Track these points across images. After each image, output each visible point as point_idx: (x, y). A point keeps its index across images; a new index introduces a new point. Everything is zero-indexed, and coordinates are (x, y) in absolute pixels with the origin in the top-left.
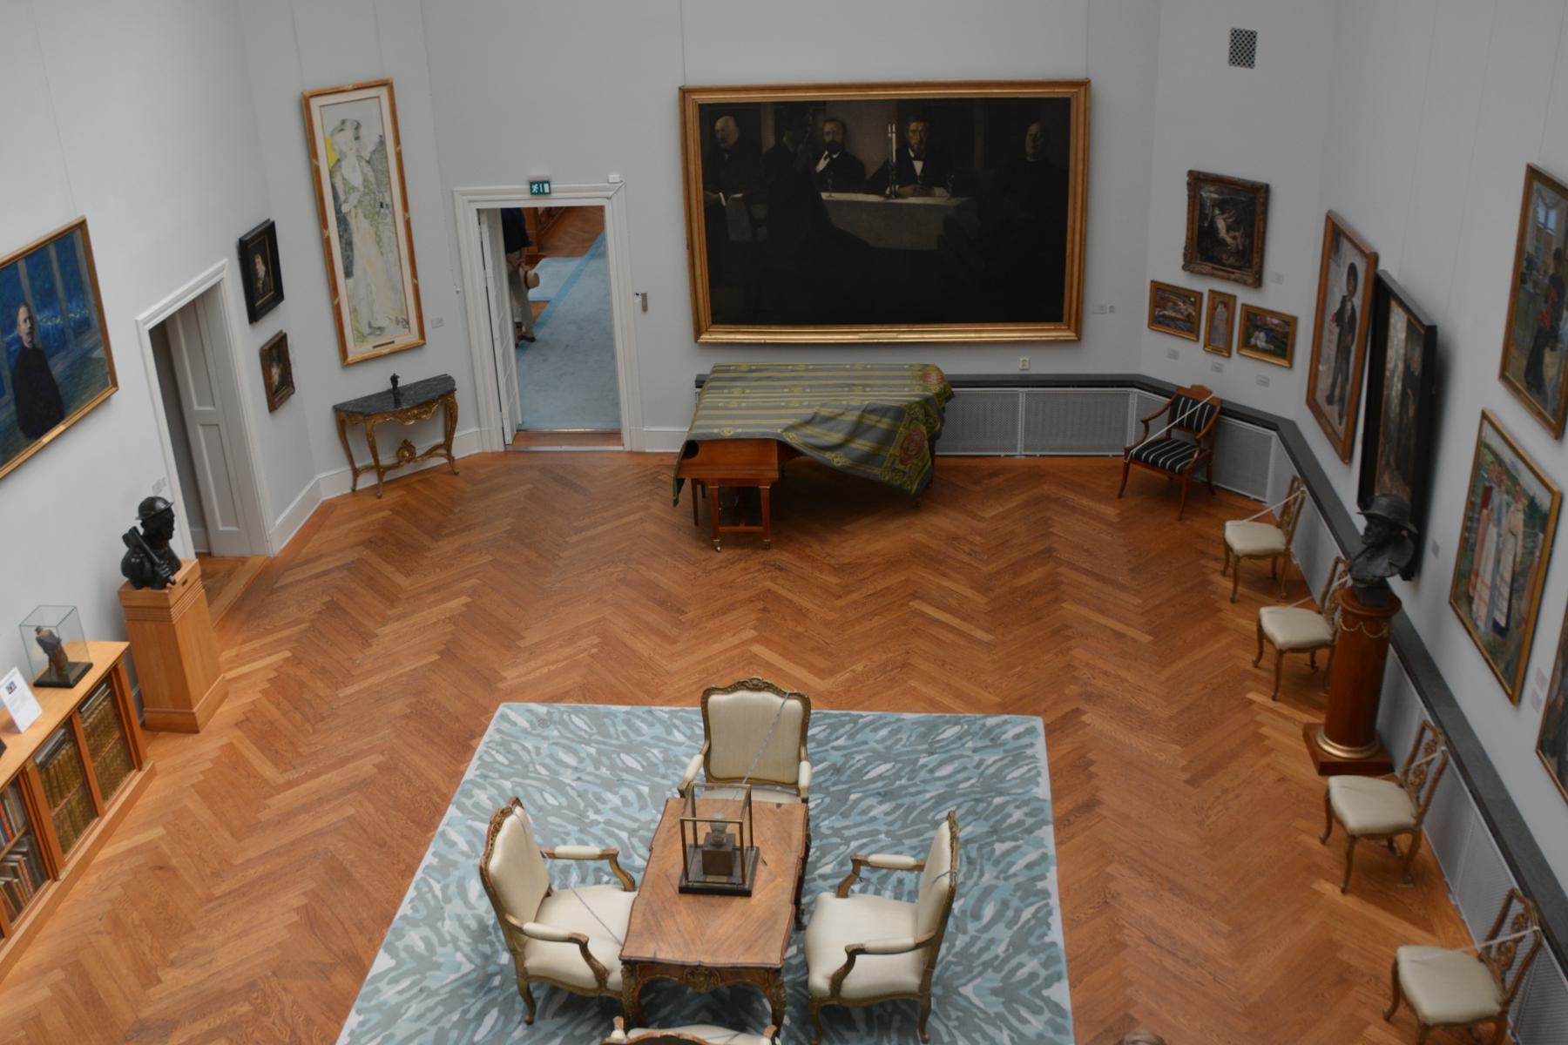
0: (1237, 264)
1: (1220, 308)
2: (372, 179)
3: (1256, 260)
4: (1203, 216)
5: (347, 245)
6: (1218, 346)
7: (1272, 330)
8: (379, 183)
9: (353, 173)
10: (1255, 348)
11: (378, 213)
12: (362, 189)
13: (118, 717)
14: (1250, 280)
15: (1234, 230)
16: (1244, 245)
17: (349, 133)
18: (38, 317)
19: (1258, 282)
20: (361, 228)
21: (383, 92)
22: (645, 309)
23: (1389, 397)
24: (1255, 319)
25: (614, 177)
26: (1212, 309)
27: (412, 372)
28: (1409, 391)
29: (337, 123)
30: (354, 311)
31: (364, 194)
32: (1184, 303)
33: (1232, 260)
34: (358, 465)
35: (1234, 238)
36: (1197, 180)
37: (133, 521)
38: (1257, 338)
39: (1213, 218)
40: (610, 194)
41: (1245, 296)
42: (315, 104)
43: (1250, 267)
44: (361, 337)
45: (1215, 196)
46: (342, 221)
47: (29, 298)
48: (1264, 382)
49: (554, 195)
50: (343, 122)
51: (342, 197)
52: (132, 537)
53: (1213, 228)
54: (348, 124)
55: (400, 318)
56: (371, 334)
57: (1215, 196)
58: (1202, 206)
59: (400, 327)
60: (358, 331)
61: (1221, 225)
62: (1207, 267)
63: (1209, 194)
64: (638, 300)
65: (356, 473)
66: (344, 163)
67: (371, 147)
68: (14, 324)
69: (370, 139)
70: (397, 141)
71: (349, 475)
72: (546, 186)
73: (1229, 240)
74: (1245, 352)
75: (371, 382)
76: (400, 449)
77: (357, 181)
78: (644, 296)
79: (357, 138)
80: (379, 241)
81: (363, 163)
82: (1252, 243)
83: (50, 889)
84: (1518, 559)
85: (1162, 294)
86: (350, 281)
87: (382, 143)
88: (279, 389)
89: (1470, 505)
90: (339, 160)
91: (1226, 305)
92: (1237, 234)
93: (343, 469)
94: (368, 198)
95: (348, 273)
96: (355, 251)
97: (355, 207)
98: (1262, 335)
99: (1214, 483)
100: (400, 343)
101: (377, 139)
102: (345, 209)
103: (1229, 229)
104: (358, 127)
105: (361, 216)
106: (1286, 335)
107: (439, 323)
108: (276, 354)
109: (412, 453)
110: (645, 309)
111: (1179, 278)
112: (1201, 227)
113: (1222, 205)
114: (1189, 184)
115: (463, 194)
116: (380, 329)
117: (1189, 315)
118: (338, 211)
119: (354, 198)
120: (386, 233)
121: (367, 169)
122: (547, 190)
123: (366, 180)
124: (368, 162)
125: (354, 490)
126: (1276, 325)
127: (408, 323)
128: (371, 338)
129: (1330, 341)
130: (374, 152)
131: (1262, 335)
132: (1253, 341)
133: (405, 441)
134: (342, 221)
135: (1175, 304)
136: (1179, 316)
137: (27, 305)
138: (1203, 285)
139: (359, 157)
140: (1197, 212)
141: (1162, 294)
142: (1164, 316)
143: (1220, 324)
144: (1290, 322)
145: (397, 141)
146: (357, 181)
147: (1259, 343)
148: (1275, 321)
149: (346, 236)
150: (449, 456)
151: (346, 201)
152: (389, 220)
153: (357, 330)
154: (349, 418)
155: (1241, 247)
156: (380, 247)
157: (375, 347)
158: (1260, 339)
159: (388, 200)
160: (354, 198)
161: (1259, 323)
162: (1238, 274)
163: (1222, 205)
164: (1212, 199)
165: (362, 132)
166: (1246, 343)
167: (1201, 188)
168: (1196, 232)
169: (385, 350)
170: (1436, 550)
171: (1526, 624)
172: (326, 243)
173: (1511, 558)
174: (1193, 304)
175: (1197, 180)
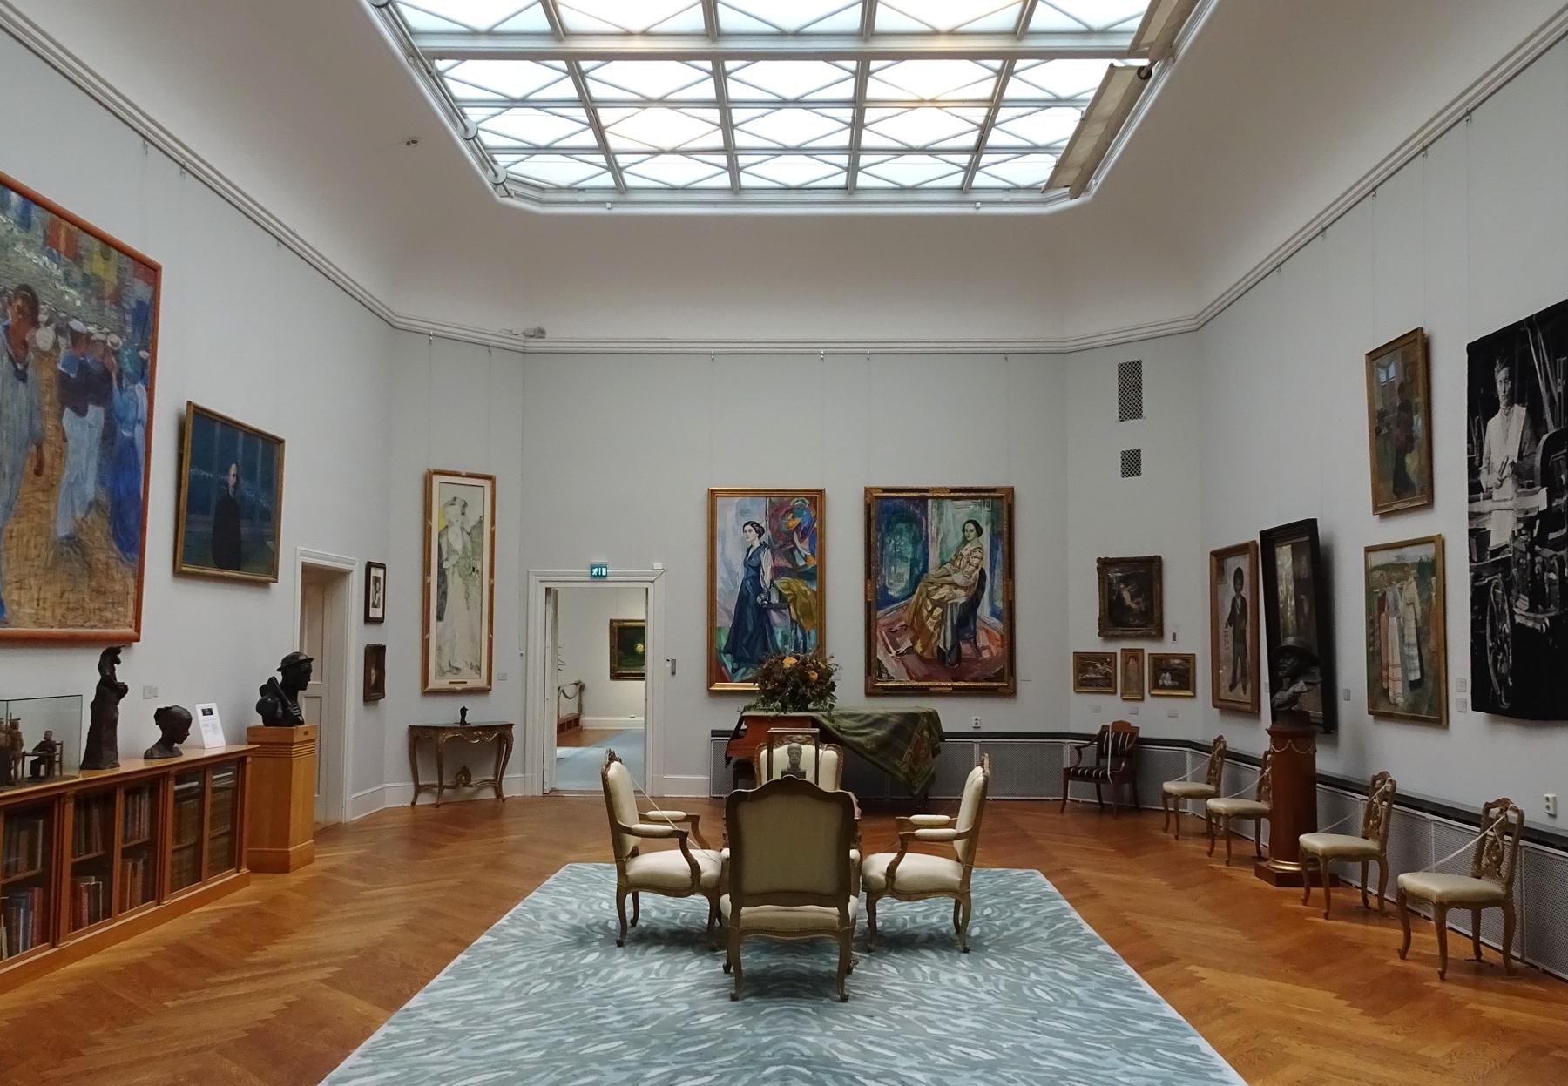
0: (1142, 623)
1: (1132, 662)
2: (470, 548)
3: (1157, 614)
4: (1111, 592)
5: (443, 594)
6: (1133, 692)
7: (1175, 669)
8: (474, 553)
9: (456, 540)
10: (1164, 687)
11: (470, 575)
12: (460, 553)
13: (234, 809)
14: (1154, 633)
15: (1137, 597)
16: (1146, 607)
17: (457, 509)
18: (242, 482)
19: (1159, 635)
20: (455, 583)
21: (487, 484)
22: (674, 673)
23: (1285, 624)
24: (1160, 664)
25: (658, 565)
26: (1125, 664)
27: (481, 712)
28: (1303, 597)
29: (450, 498)
30: (439, 649)
31: (461, 558)
32: (1102, 664)
33: (1137, 622)
34: (421, 783)
35: (1138, 603)
36: (1105, 565)
37: (272, 670)
38: (1164, 678)
39: (1120, 591)
40: (652, 578)
41: (1150, 648)
42: (437, 479)
43: (1152, 623)
44: (441, 672)
45: (1120, 574)
46: (442, 574)
47: (239, 461)
48: (1174, 716)
49: (609, 578)
50: (455, 499)
51: (445, 556)
52: (268, 689)
53: (1120, 599)
54: (458, 500)
55: (474, 664)
56: (449, 671)
57: (1120, 574)
58: (1110, 584)
59: (473, 672)
60: (440, 667)
61: (1126, 596)
62: (1118, 632)
63: (1115, 574)
64: (669, 665)
65: (419, 789)
66: (450, 530)
67: (473, 524)
68: (227, 471)
69: (472, 519)
70: (493, 523)
71: (412, 791)
72: (604, 570)
73: (1133, 605)
74: (1155, 692)
75: (442, 713)
76: (459, 773)
77: (458, 546)
78: (674, 662)
79: (463, 514)
80: (467, 598)
81: (465, 534)
82: (1152, 605)
83: (152, 909)
84: (1418, 617)
85: (1084, 662)
86: (441, 623)
87: (481, 522)
88: (374, 690)
89: (1369, 611)
90: (447, 527)
91: (1136, 658)
92: (1140, 600)
93: (407, 784)
94: (464, 561)
95: (440, 618)
96: (448, 599)
97: (454, 566)
98: (1168, 675)
99: (1142, 806)
100: (471, 684)
101: (478, 518)
102: (445, 565)
103: (1132, 599)
104: (465, 505)
105: (456, 574)
106: (1187, 671)
107: (503, 678)
108: (375, 656)
109: (469, 780)
110: (674, 673)
111: (1095, 645)
112: (1110, 601)
113: (1125, 580)
114: (1098, 568)
115: (536, 575)
116: (457, 669)
117: (1107, 674)
118: (440, 565)
119: (454, 559)
120: (474, 592)
121: (467, 538)
122: (604, 573)
123: (464, 547)
124: (469, 534)
125: (413, 804)
126: (1178, 664)
127: (480, 669)
128: (449, 675)
129: (1227, 642)
130: (474, 527)
131: (1168, 675)
132: (1161, 682)
133: (464, 767)
134: (442, 574)
135: (1095, 667)
136: (1099, 676)
137: (237, 464)
138: (1115, 648)
139: (462, 528)
140: (1107, 589)
141: (1084, 662)
142: (1086, 679)
143: (1133, 675)
144: (1189, 660)
145: (493, 523)
146: (458, 546)
147: (1166, 682)
148: (1177, 661)
149: (443, 586)
150: (499, 794)
151: (447, 560)
152: (478, 583)
153: (439, 665)
154: (421, 738)
155: (1143, 609)
156: (468, 602)
157: (451, 683)
158: (1167, 679)
159: (479, 567)
160: (454, 559)
161: (1165, 666)
162: (1143, 630)
163: (1125, 580)
164: (1116, 577)
165: (467, 510)
166: (1156, 685)
167: (1108, 571)
168: (1107, 606)
169: (459, 687)
170: (1348, 692)
171: (1438, 655)
172: (426, 588)
173: (1413, 624)
174: (1109, 664)
175: (1105, 565)
